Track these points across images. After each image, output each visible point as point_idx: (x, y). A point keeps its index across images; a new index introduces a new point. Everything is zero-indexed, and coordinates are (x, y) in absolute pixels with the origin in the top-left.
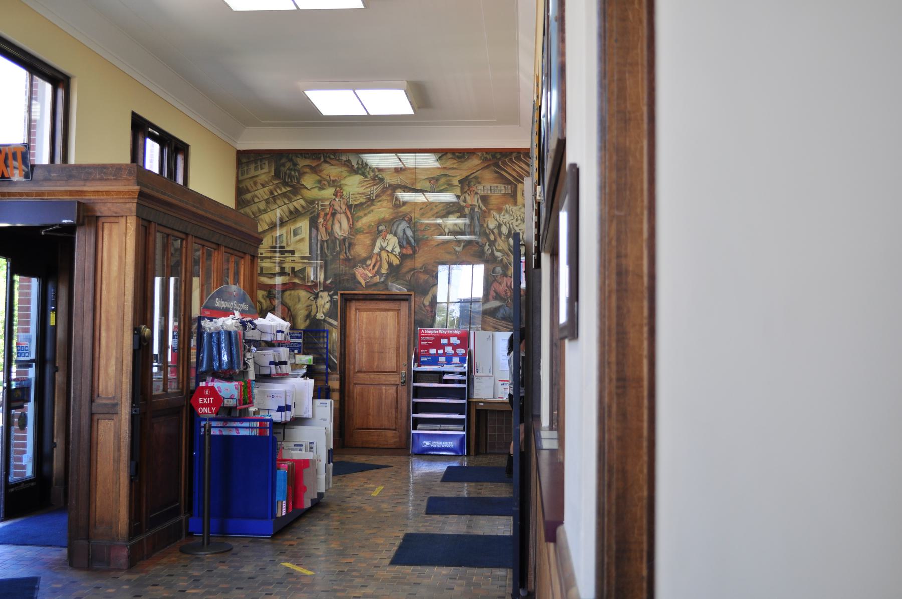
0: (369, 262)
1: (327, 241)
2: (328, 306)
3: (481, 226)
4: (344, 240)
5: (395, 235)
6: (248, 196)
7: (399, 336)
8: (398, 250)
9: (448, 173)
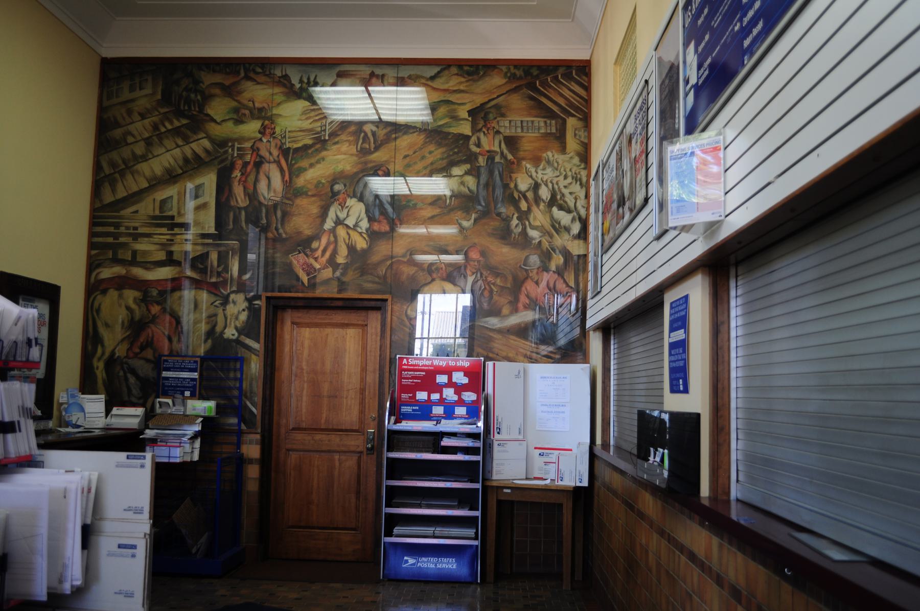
0: (315, 245)
1: (245, 208)
2: (243, 317)
3: (506, 186)
4: (275, 206)
5: (361, 199)
6: (117, 133)
7: (364, 369)
8: (365, 224)
9: (453, 98)
